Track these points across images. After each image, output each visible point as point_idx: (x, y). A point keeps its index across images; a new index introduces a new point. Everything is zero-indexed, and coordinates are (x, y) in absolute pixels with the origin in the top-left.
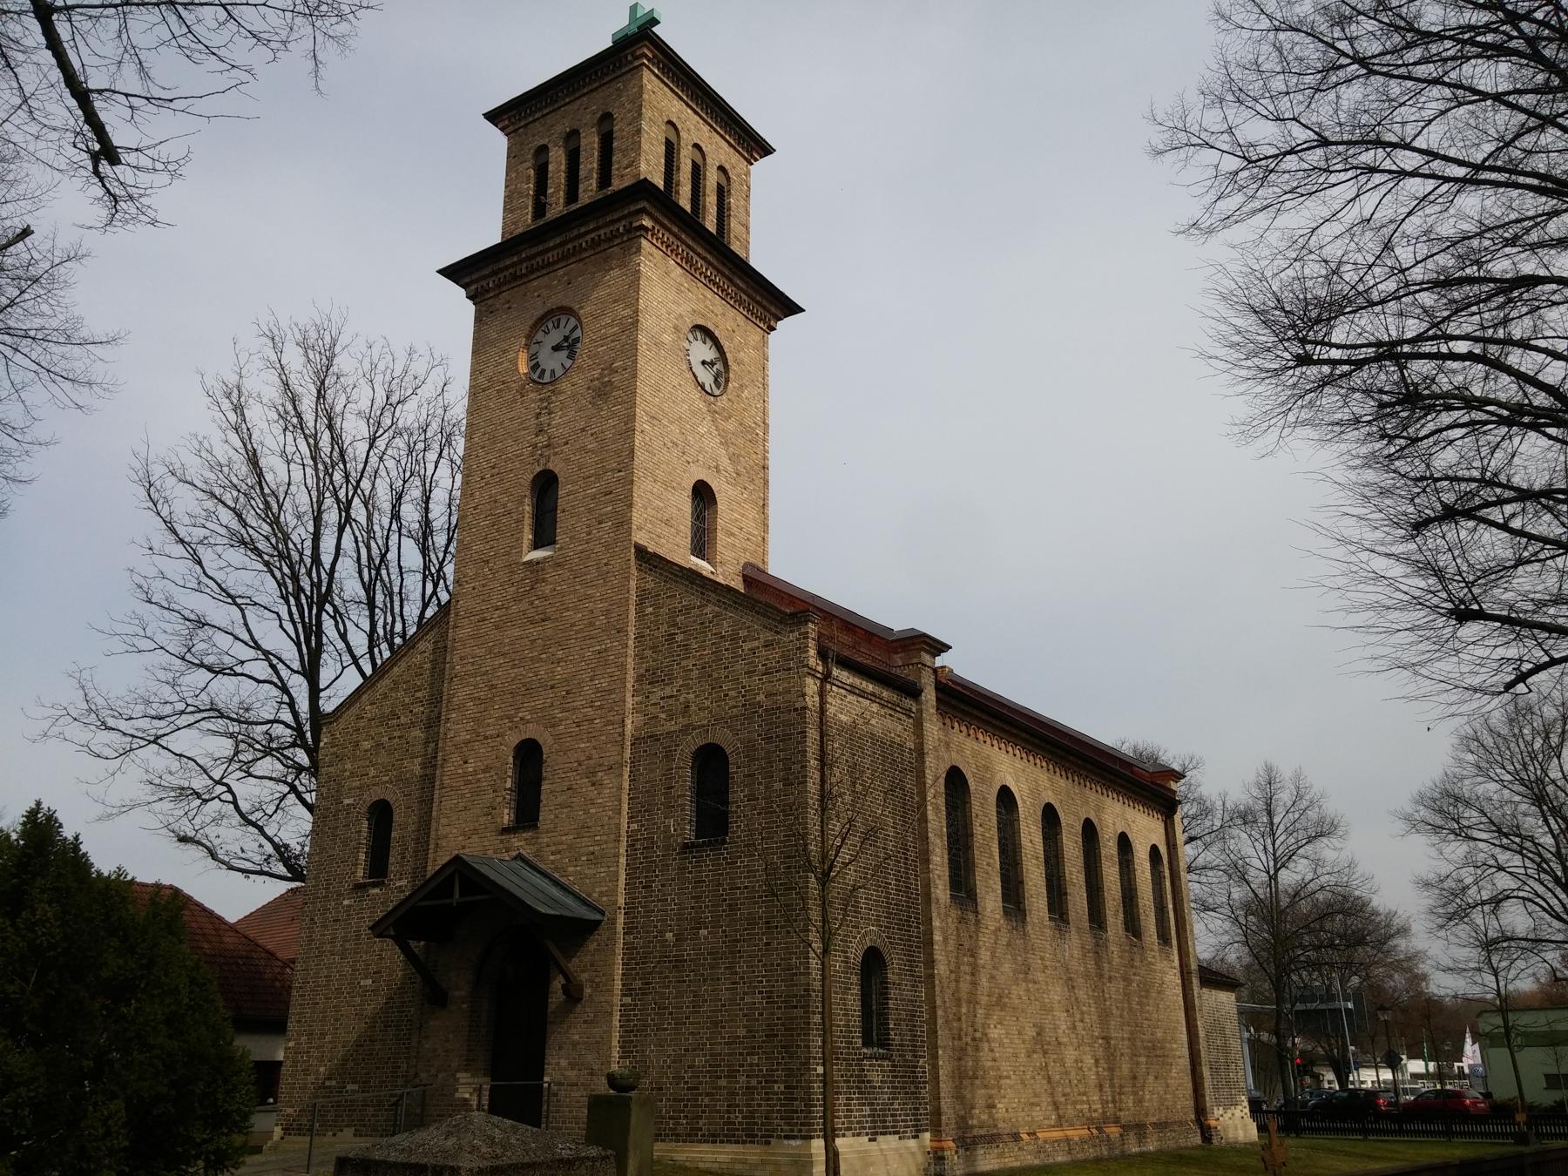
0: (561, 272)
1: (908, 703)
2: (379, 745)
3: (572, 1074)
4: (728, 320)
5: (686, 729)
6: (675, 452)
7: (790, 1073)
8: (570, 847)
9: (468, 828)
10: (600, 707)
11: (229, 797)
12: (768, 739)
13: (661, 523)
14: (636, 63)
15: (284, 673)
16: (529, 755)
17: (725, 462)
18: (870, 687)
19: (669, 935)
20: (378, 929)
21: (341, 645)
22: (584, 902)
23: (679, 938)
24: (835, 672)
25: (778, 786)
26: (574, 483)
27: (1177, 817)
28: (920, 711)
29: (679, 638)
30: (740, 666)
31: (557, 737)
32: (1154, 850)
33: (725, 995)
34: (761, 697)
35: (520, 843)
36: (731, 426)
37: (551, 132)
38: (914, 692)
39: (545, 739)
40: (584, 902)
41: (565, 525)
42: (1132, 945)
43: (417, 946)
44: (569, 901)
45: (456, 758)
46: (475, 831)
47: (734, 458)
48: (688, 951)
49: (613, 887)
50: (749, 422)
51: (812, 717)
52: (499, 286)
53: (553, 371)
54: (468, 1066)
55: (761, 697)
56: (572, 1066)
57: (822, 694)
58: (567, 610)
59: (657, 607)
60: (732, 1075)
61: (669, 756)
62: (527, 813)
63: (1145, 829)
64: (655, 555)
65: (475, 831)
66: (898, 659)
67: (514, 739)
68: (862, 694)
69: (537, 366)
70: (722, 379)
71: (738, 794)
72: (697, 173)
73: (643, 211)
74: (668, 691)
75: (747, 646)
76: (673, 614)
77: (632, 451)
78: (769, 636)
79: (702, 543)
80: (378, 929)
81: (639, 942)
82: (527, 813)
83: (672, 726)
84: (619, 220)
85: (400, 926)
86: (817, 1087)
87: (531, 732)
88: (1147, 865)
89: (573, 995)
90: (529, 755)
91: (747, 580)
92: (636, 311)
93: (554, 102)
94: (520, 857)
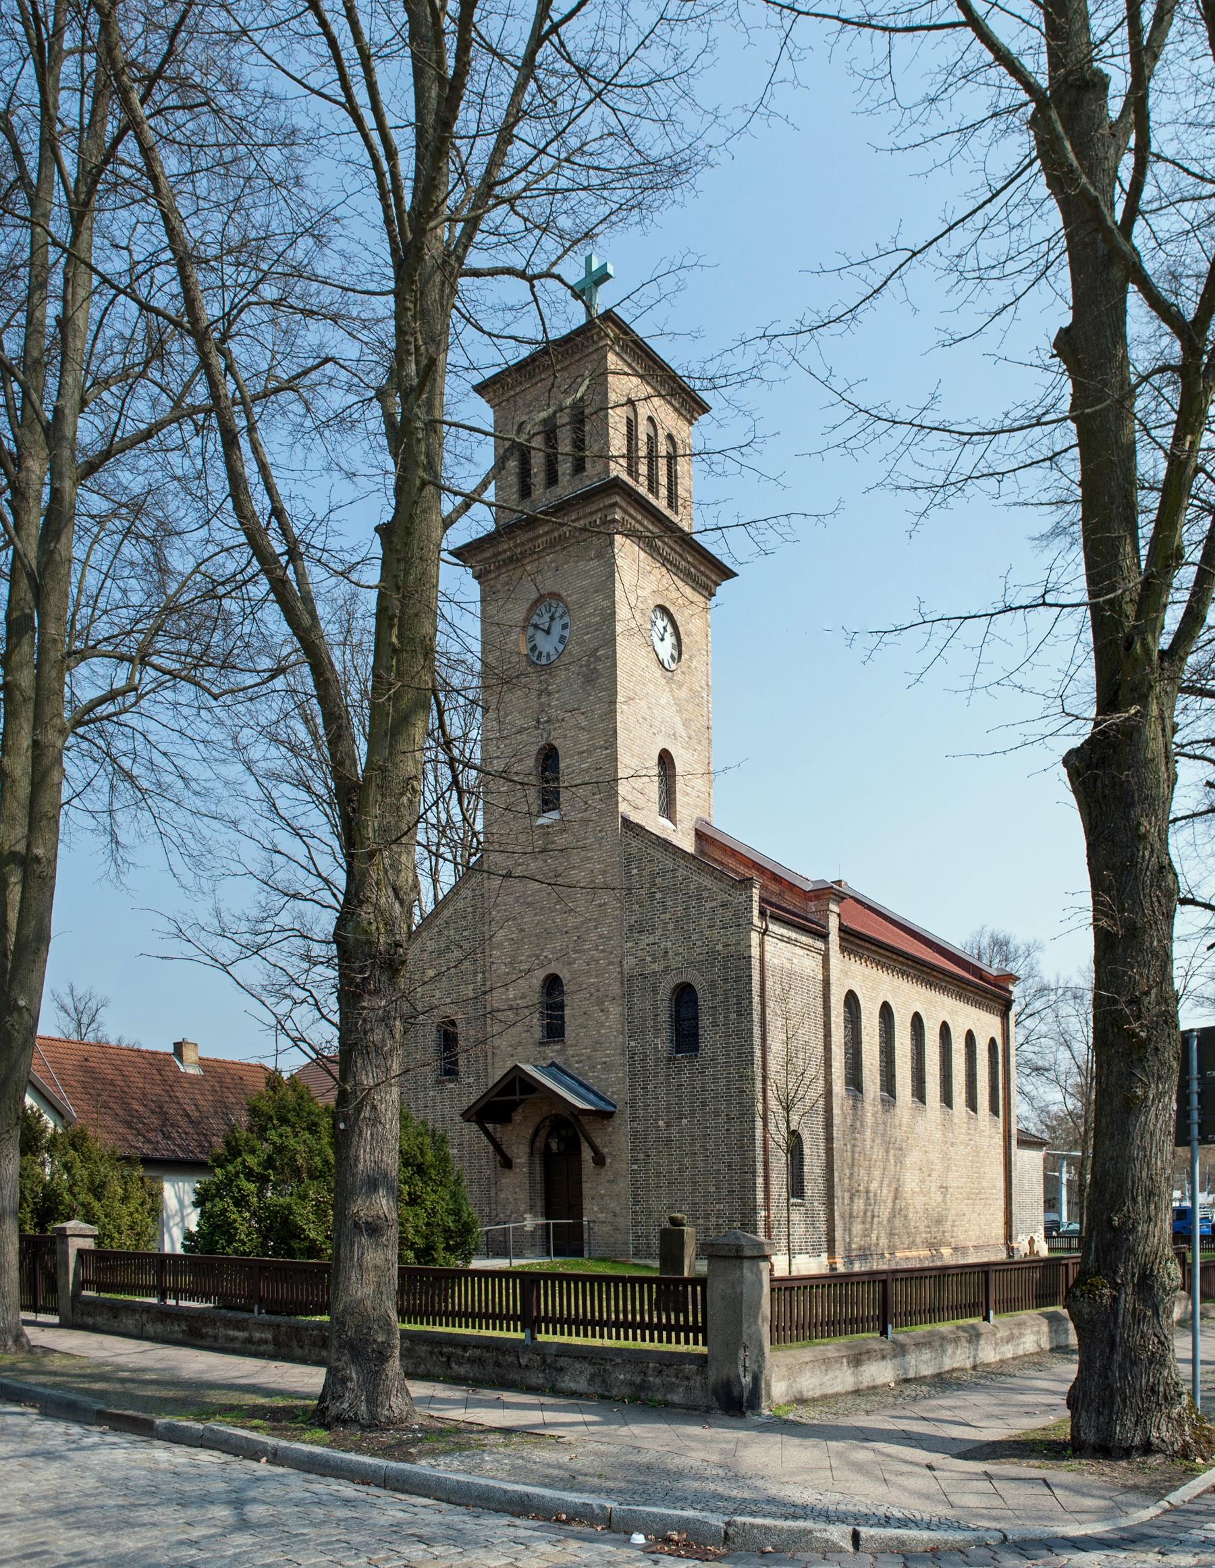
0: (548, 559)
1: (820, 945)
3: (602, 1216)
4: (679, 595)
5: (666, 971)
6: (646, 726)
7: (744, 1216)
8: (589, 1057)
10: (603, 951)
11: (311, 1000)
12: (725, 980)
13: (638, 800)
14: (602, 343)
17: (681, 730)
18: (793, 935)
19: (661, 1123)
20: (467, 1116)
22: (602, 1099)
23: (668, 1126)
24: (771, 927)
25: (733, 1016)
26: (571, 756)
27: (1012, 1014)
28: (827, 949)
29: (658, 895)
30: (704, 922)
31: (573, 972)
32: (993, 1041)
33: (700, 1164)
34: (720, 947)
35: (552, 1052)
36: (683, 693)
38: (824, 937)
39: (565, 975)
40: (602, 1099)
42: (970, 1118)
46: (520, 1044)
47: (686, 724)
48: (675, 1135)
49: (615, 1085)
50: (696, 687)
51: (755, 963)
52: (499, 568)
53: (548, 655)
54: (532, 1209)
55: (720, 947)
56: (601, 1210)
57: (762, 944)
58: (573, 868)
59: (641, 870)
60: (707, 1217)
61: (655, 991)
62: (554, 1031)
63: (986, 1025)
64: (638, 825)
65: (520, 1044)
66: (812, 906)
67: (541, 974)
68: (789, 941)
69: (534, 648)
70: (678, 656)
71: (705, 1021)
72: (652, 441)
73: (615, 504)
74: (651, 939)
75: (709, 905)
76: (653, 876)
77: (615, 732)
78: (726, 897)
79: (668, 807)
81: (640, 1128)
82: (554, 1031)
83: (656, 967)
84: (596, 512)
87: (554, 968)
88: (986, 1055)
89: (599, 1160)
90: (553, 984)
91: (700, 836)
92: (613, 603)
93: (532, 377)
94: (553, 1064)
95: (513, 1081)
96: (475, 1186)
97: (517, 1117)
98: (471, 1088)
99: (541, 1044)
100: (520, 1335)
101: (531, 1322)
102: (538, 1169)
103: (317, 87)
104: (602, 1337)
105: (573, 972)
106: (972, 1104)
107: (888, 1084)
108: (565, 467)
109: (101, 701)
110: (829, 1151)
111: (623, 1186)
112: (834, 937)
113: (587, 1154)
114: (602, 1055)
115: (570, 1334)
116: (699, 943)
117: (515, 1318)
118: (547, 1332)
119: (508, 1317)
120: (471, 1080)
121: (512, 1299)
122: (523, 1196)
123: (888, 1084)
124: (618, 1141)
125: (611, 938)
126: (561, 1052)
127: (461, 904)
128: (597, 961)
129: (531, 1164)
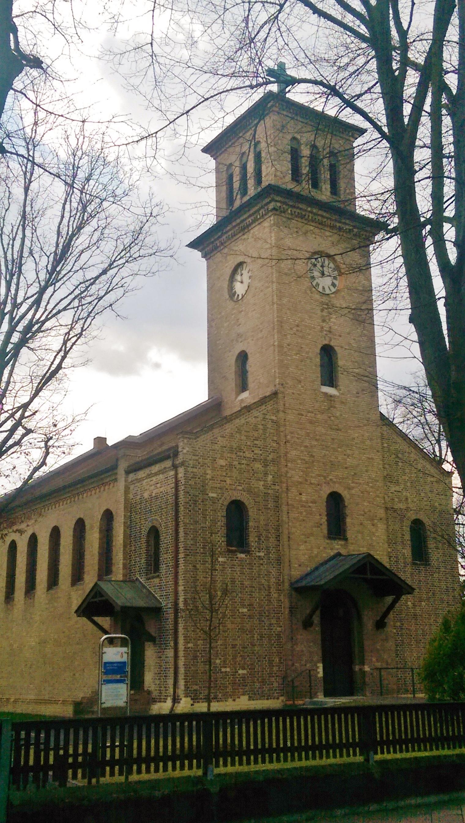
10: (372, 487)
19: (409, 603)
23: (414, 605)
30: (427, 488)
39: (345, 494)
55: (437, 504)
56: (378, 661)
67: (326, 491)
74: (397, 488)
95: (365, 565)
96: (265, 641)
100: (359, 759)
101: (368, 745)
104: (382, 753)
105: (352, 495)
109: (381, 141)
115: (300, 759)
116: (425, 499)
117: (354, 745)
118: (382, 753)
119: (348, 746)
120: (262, 554)
121: (353, 730)
125: (377, 481)
126: (345, 546)
128: (369, 493)
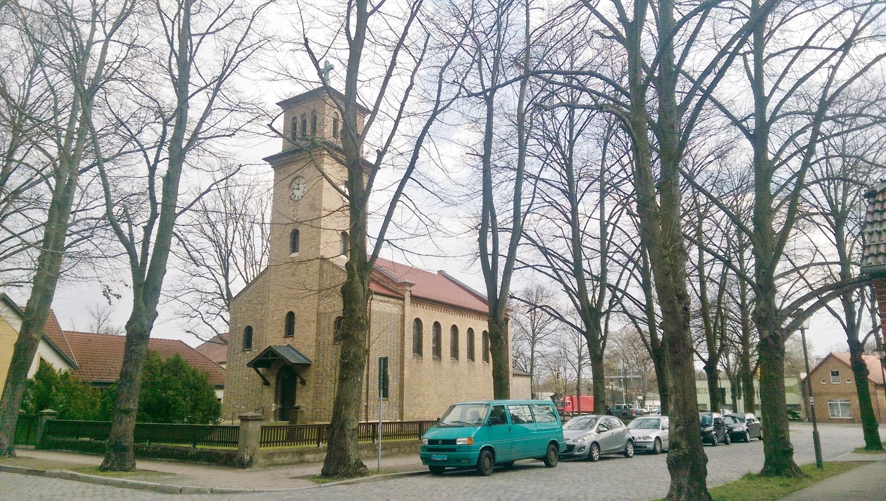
1: (401, 302)
2: (248, 310)
9: (271, 337)
15: (216, 275)
16: (291, 316)
20: (249, 365)
21: (235, 268)
35: (288, 341)
37: (299, 111)
38: (403, 299)
39: (295, 311)
41: (301, 246)
43: (260, 369)
44: (302, 358)
45: (270, 315)
62: (290, 330)
66: (399, 288)
67: (287, 311)
68: (385, 301)
80: (249, 365)
82: (290, 330)
85: (255, 364)
86: (364, 408)
89: (303, 382)
90: (291, 316)
97: (273, 365)
98: (256, 352)
99: (285, 337)
102: (280, 386)
103: (405, 190)
106: (471, 356)
107: (437, 351)
108: (299, 120)
110: (402, 380)
111: (311, 393)
112: (408, 299)
113: (299, 380)
114: (310, 343)
122: (272, 396)
123: (437, 351)
124: (311, 376)
127: (259, 284)
129: (277, 384)
